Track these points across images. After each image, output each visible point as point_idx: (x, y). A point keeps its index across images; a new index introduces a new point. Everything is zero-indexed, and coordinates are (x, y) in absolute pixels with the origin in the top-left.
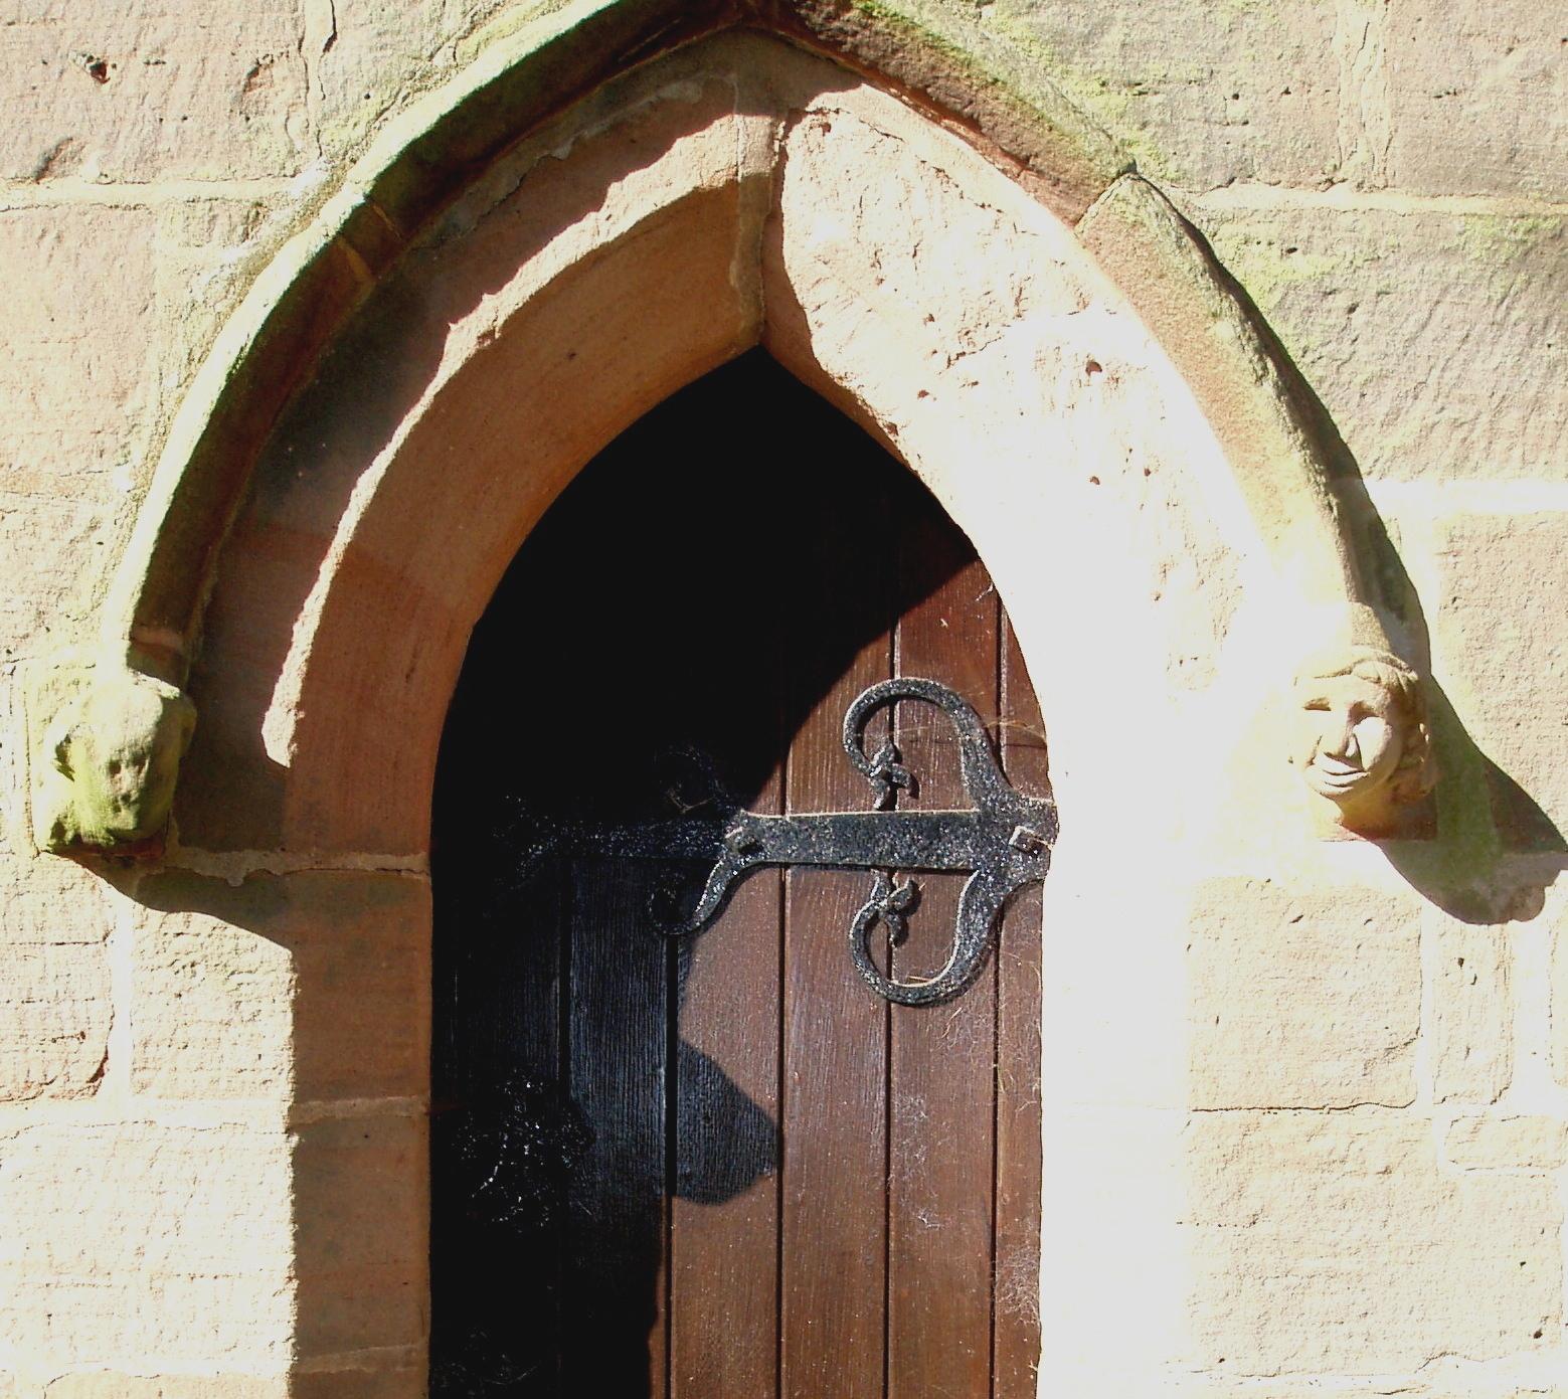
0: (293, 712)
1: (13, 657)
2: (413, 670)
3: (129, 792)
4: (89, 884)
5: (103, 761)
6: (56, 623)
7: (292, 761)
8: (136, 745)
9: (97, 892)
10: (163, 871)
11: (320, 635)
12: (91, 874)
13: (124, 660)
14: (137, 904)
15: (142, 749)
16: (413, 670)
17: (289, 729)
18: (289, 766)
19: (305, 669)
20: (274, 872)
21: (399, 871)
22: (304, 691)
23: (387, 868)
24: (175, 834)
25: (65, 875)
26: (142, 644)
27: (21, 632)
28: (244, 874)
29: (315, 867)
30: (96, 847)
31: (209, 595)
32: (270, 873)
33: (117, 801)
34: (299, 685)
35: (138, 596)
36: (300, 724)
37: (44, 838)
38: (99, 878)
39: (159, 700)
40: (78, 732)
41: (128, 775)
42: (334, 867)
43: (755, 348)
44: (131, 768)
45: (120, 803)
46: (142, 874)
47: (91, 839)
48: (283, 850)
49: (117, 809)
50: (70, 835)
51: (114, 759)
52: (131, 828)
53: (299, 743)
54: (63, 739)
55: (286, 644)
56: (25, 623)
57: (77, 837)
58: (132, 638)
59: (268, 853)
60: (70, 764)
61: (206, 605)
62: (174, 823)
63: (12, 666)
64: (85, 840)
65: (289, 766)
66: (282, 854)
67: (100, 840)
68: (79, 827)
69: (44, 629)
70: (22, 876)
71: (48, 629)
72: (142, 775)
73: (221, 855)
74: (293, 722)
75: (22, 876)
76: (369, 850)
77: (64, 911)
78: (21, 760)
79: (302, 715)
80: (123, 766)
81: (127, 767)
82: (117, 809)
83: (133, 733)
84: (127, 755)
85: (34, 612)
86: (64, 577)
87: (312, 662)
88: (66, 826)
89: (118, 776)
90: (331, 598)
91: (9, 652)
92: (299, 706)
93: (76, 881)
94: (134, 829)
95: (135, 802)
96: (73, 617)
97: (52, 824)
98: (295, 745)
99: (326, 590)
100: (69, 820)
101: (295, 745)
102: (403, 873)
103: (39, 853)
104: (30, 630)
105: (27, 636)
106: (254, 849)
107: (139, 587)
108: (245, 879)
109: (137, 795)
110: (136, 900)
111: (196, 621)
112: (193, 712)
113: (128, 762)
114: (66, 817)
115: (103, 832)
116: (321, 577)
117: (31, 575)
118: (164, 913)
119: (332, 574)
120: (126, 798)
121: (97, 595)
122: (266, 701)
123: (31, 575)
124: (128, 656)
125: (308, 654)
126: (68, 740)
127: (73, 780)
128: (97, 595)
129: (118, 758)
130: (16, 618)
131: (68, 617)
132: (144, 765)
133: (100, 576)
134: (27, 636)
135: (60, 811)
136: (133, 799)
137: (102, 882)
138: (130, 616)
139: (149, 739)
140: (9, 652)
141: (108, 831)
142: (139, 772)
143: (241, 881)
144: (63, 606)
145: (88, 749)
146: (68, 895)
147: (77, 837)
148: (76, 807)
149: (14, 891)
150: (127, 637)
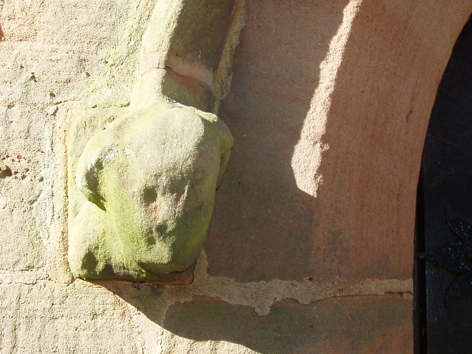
0: (318, 145)
1: (57, 99)
2: (411, 112)
3: (165, 222)
4: (119, 310)
5: (137, 187)
6: (95, 69)
7: (318, 192)
8: (175, 169)
9: (127, 318)
10: (190, 299)
11: (342, 71)
12: (121, 300)
13: (159, 87)
14: (165, 330)
15: (181, 173)
16: (411, 112)
17: (315, 161)
18: (316, 196)
19: (329, 103)
20: (300, 301)
21: (401, 293)
22: (329, 125)
23: (392, 291)
24: (204, 263)
25: (97, 301)
26: (177, 74)
27: (64, 77)
28: (271, 303)
29: (338, 295)
30: (128, 278)
31: (237, 37)
32: (297, 301)
33: (151, 232)
34: (324, 119)
35: (174, 26)
36: (325, 155)
37: (76, 266)
38: (129, 305)
39: (201, 122)
40: (111, 156)
41: (163, 203)
42: (354, 293)
43: (87, 254)
44: (168, 195)
45: (155, 234)
46: (171, 302)
47: (122, 271)
48: (310, 279)
49: (151, 241)
50: (100, 266)
51: (150, 185)
52: (166, 262)
53: (324, 175)
54: (94, 162)
55: (315, 82)
56: (68, 69)
57: (108, 267)
58: (167, 68)
59: (296, 282)
60: (102, 192)
61: (234, 47)
62: (203, 252)
63: (55, 107)
64: (116, 271)
65: (316, 196)
66: (310, 283)
67: (131, 272)
68: (110, 259)
69: (84, 74)
70: (57, 301)
71: (88, 75)
72: (181, 203)
73: (248, 284)
74: (319, 153)
75: (57, 301)
76: (380, 276)
77: (95, 335)
78: (60, 193)
79: (326, 147)
80: (159, 194)
81: (164, 194)
82: (151, 241)
83: (171, 155)
84: (164, 181)
85: (75, 59)
86: (104, 28)
87: (335, 97)
88: (98, 257)
89: (153, 205)
90: (351, 38)
91: (52, 95)
92: (325, 139)
93: (108, 306)
94: (169, 263)
95: (171, 233)
96: (111, 62)
97: (82, 255)
98: (321, 176)
99: (348, 30)
100: (100, 251)
101: (321, 176)
102: (405, 295)
103: (73, 280)
104: (72, 75)
105: (69, 81)
106: (282, 278)
107: (175, 18)
108: (272, 308)
109: (173, 226)
110: (164, 327)
111: (225, 62)
112: (229, 139)
113: (165, 188)
114: (97, 248)
115: (135, 265)
116: (345, 19)
117: (75, 28)
118: (192, 341)
119: (353, 16)
120: (161, 229)
121: (132, 43)
122: (295, 136)
123: (75, 28)
124: (163, 84)
125: (331, 90)
126: (99, 165)
127: (104, 209)
128: (132, 43)
129: (154, 184)
130: (60, 66)
131: (107, 62)
132: (183, 193)
133: (135, 26)
134: (69, 81)
135: (91, 242)
136: (169, 229)
137: (131, 307)
138: (166, 45)
139: (190, 162)
140: (52, 95)
141: (141, 264)
142: (177, 200)
143: (267, 311)
144: (102, 54)
145: (121, 175)
146: (100, 321)
147: (108, 267)
148: (108, 237)
149: (49, 315)
150: (162, 66)
